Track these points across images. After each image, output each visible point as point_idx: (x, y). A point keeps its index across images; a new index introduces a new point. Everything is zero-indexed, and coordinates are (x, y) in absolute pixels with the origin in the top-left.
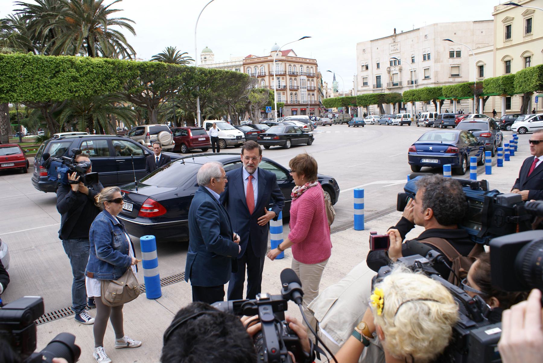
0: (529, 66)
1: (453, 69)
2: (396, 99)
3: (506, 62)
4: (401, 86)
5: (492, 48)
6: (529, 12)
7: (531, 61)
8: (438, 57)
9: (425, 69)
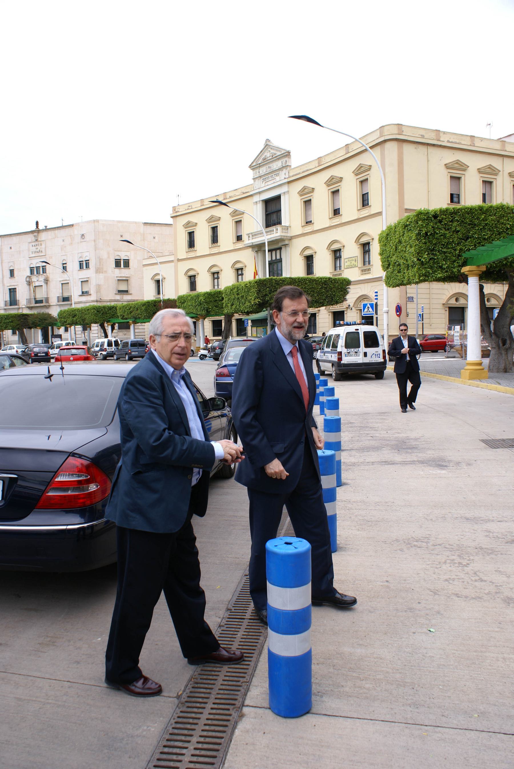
0: (242, 280)
1: (120, 282)
2: (46, 321)
3: (190, 277)
4: (47, 304)
5: (172, 258)
6: (214, 218)
7: (220, 278)
8: (100, 265)
9: (82, 282)
